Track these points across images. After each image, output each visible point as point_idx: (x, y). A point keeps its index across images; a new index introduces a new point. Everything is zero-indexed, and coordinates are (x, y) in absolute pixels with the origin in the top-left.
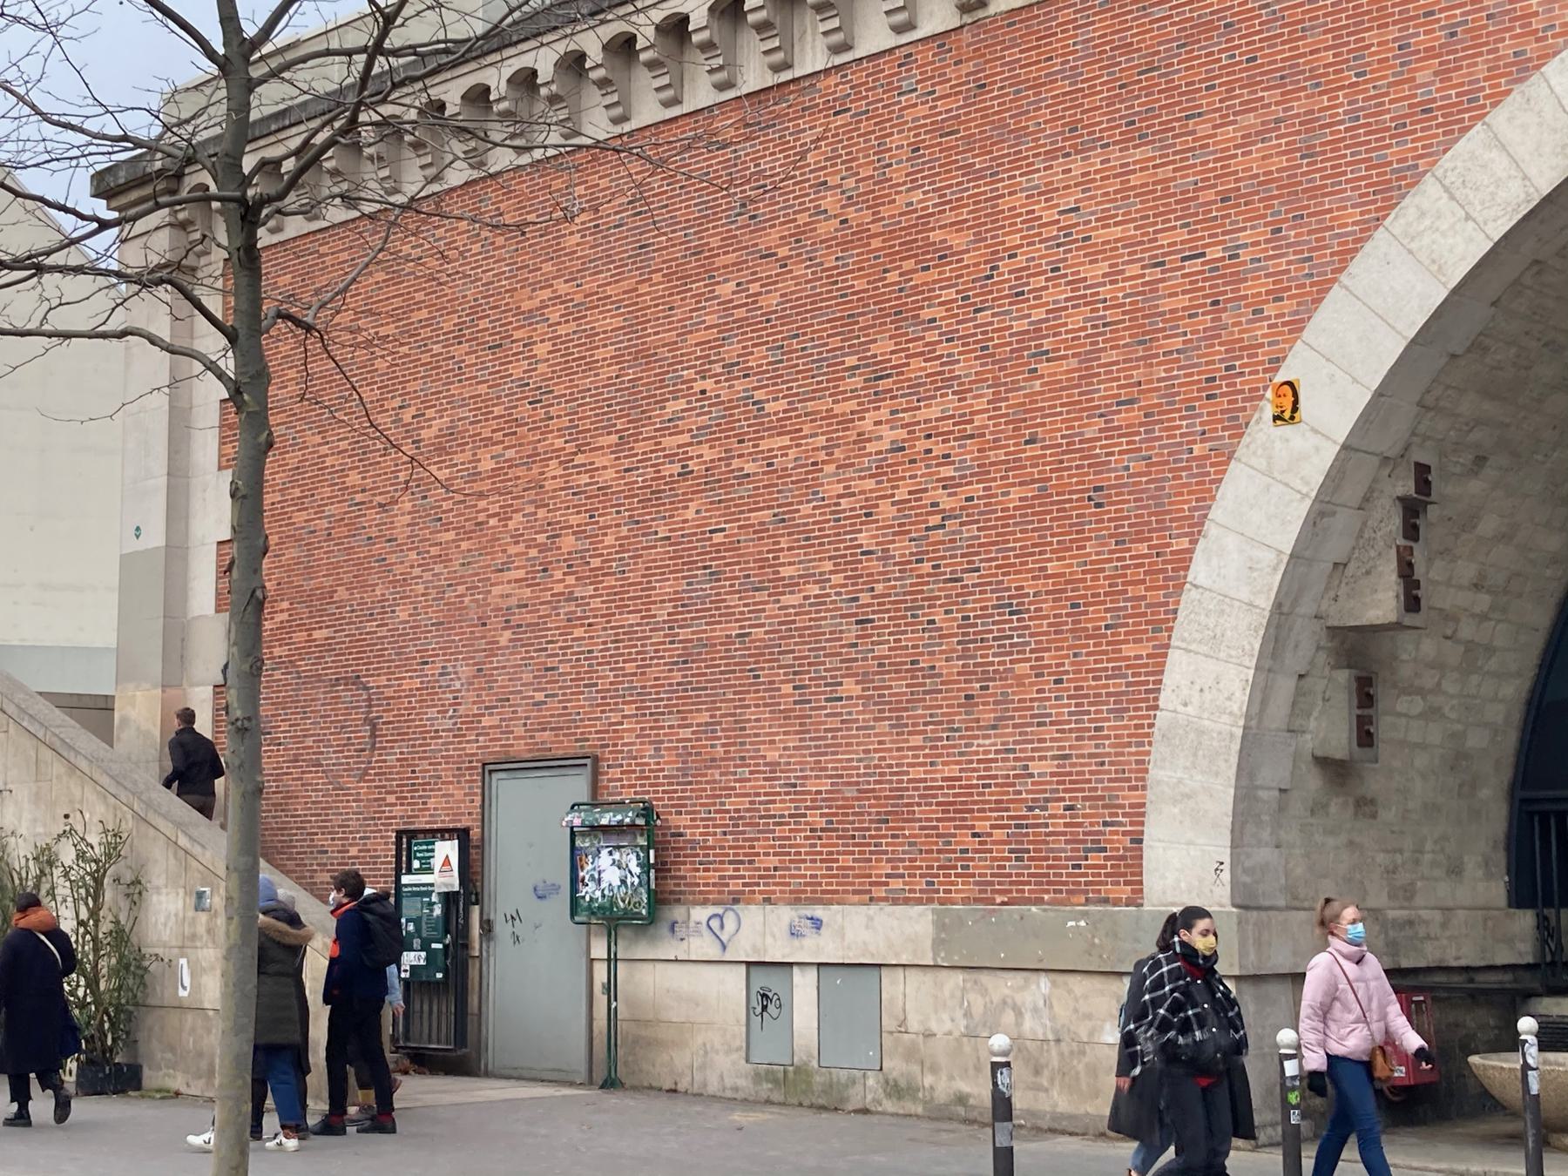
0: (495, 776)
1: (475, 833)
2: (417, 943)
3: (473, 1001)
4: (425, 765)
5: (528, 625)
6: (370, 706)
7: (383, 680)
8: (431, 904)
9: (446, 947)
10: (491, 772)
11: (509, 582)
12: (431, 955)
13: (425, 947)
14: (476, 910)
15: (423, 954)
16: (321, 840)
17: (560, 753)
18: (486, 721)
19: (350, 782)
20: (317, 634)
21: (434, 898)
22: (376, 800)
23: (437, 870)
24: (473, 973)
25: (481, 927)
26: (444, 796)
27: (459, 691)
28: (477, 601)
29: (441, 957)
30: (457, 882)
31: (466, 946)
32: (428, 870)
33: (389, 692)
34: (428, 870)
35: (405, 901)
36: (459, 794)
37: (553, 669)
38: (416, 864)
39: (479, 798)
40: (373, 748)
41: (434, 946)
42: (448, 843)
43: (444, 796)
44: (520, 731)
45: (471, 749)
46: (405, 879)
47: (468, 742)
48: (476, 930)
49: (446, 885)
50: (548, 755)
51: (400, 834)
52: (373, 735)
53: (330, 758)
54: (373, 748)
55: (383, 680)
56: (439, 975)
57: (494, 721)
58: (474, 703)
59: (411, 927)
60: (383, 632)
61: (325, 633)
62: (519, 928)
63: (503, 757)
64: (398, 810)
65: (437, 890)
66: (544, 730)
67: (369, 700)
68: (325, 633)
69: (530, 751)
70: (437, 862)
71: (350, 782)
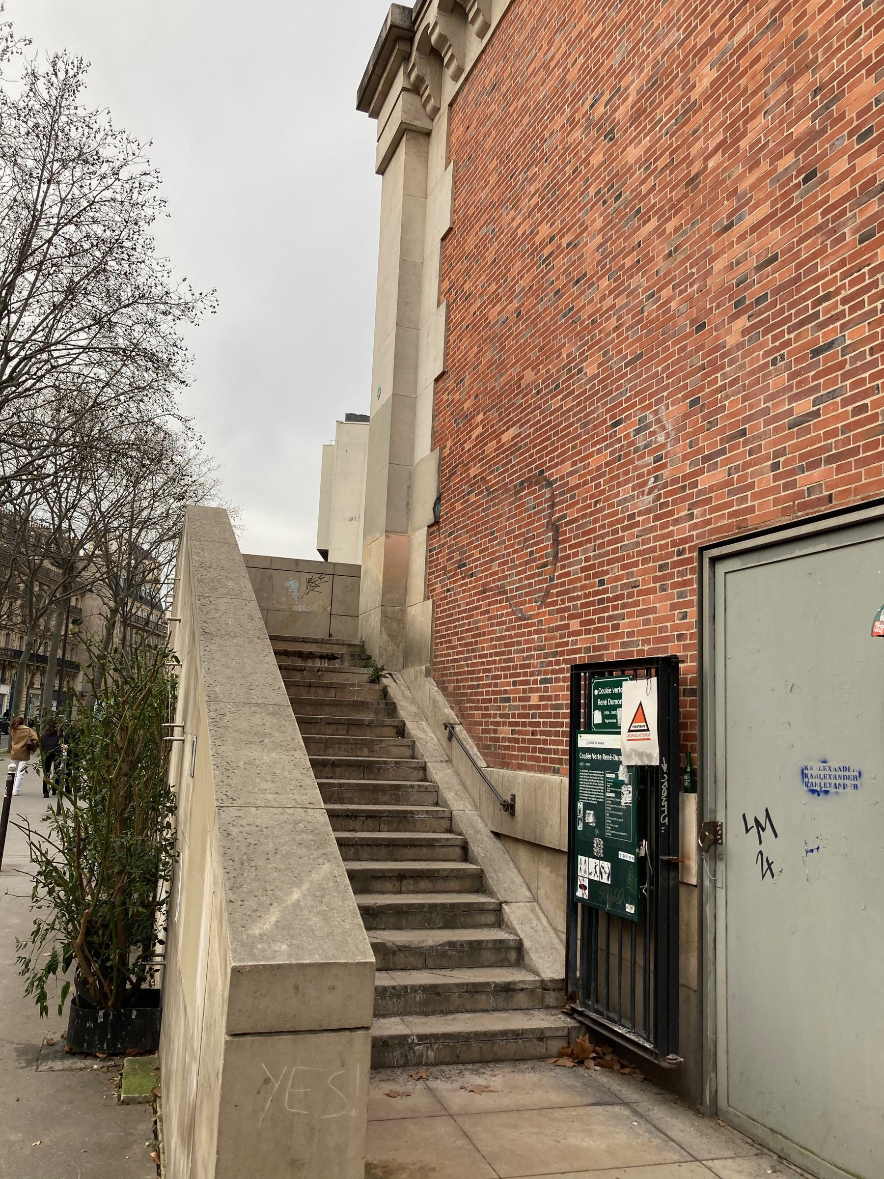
0: (722, 568)
1: (687, 667)
2: (598, 844)
3: (689, 963)
4: (616, 570)
5: (776, 291)
6: (552, 506)
7: (567, 467)
8: (618, 784)
9: (640, 860)
10: (714, 561)
11: (742, 237)
12: (618, 867)
13: (609, 855)
14: (690, 804)
15: (607, 866)
16: (505, 685)
17: (855, 500)
18: (705, 481)
19: (530, 608)
20: (505, 438)
21: (623, 775)
22: (558, 628)
23: (624, 729)
24: (688, 914)
25: (701, 835)
26: (641, 613)
27: (663, 446)
28: (690, 298)
29: (632, 878)
30: (655, 751)
31: (675, 867)
32: (611, 727)
33: (573, 481)
34: (611, 727)
35: (582, 773)
36: (662, 607)
37: (830, 345)
38: (597, 717)
39: (693, 611)
40: (556, 559)
41: (623, 855)
42: (642, 683)
43: (641, 613)
44: (766, 480)
45: (682, 530)
46: (584, 740)
47: (676, 522)
48: (691, 839)
49: (640, 755)
50: (836, 506)
51: (577, 669)
52: (556, 542)
53: (513, 582)
54: (556, 559)
55: (567, 467)
56: (630, 909)
57: (719, 475)
58: (685, 458)
59: (590, 819)
60: (570, 403)
61: (512, 432)
62: (771, 845)
63: (735, 533)
64: (582, 642)
65: (625, 762)
66: (815, 465)
67: (553, 496)
68: (512, 432)
69: (785, 511)
70: (625, 716)
71: (530, 608)
